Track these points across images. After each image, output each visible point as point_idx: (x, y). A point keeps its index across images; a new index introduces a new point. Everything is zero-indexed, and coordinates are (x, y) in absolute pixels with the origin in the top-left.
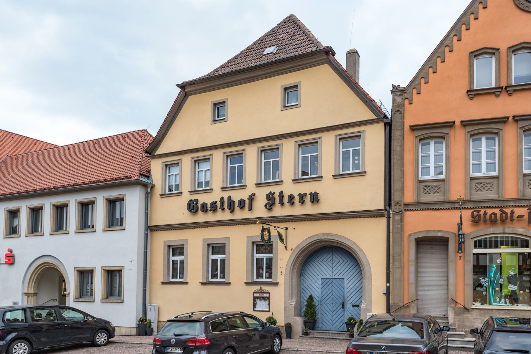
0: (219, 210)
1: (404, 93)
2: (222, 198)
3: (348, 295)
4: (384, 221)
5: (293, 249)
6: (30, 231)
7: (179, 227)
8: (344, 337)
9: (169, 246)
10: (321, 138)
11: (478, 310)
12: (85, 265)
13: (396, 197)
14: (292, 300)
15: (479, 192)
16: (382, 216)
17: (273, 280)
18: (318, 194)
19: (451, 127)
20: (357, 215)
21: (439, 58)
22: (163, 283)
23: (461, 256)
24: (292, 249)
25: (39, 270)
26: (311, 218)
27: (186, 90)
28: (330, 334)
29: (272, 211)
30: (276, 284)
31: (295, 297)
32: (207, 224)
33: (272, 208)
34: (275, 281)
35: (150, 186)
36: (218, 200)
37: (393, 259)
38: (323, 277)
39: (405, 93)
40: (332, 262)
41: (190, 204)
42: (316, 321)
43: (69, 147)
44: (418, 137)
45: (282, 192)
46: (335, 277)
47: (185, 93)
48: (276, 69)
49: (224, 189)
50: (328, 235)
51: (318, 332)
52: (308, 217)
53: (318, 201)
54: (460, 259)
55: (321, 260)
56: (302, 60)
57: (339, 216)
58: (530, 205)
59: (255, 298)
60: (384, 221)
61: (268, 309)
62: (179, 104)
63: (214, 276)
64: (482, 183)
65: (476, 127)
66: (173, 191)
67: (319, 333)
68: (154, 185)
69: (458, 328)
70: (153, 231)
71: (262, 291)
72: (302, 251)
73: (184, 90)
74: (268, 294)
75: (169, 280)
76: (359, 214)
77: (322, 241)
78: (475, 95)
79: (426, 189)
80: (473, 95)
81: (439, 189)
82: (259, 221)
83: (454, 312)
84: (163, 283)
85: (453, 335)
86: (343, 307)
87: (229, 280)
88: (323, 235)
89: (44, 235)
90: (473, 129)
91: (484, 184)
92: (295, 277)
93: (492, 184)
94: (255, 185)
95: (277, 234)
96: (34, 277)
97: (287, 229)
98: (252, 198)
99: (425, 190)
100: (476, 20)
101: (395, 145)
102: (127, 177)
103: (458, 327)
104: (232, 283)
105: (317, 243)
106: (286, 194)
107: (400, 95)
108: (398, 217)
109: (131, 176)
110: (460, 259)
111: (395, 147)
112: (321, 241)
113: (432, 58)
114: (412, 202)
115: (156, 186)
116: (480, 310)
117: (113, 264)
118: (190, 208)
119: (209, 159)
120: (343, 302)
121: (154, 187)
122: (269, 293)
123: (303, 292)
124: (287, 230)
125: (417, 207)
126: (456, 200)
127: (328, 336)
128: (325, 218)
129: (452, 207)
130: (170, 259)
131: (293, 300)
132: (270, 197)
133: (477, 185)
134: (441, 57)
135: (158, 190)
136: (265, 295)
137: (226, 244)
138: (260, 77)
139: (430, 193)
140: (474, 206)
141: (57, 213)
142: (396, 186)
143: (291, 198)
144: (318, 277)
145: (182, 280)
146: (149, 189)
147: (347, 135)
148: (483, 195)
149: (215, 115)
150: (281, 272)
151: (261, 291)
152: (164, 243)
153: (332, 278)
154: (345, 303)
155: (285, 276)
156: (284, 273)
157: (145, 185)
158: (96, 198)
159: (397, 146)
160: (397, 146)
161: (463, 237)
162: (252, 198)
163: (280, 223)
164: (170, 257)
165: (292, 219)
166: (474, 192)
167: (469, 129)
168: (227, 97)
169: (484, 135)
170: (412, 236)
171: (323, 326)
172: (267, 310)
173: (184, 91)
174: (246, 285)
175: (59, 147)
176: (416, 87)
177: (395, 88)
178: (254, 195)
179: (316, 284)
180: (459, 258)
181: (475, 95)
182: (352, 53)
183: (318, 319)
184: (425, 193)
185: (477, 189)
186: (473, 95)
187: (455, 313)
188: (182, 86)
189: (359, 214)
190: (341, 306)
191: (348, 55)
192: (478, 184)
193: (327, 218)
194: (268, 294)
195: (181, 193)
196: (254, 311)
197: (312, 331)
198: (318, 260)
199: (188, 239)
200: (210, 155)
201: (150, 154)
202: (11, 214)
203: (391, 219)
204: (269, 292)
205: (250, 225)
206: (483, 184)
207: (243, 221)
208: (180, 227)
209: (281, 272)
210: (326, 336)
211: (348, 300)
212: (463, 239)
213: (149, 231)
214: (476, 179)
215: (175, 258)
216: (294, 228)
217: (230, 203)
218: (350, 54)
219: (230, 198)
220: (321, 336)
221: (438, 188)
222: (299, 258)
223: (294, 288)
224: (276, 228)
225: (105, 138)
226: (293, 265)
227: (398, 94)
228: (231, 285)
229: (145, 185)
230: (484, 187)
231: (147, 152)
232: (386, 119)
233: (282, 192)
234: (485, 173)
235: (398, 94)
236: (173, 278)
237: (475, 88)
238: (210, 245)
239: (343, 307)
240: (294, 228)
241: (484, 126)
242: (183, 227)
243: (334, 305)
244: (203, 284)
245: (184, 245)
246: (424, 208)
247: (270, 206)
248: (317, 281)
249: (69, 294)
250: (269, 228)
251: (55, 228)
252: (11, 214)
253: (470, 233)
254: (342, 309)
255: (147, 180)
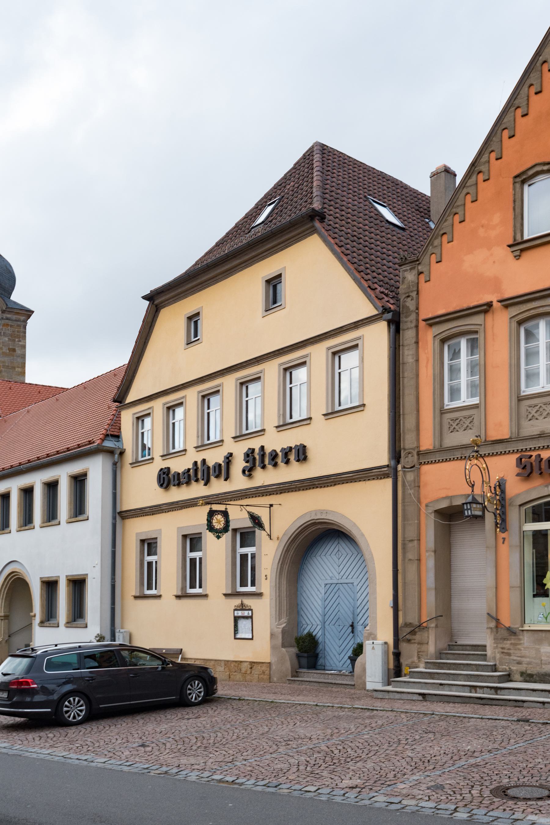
0: (281, 465)
1: (417, 265)
2: (196, 463)
3: (359, 610)
4: (388, 482)
5: (280, 537)
6: (46, 519)
7: (150, 511)
8: (347, 681)
9: (185, 537)
10: (309, 355)
11: (530, 632)
12: (49, 574)
13: (408, 441)
14: (279, 620)
15: (533, 422)
16: (385, 476)
17: (256, 588)
18: (306, 446)
19: (486, 312)
20: (354, 477)
21: (468, 195)
22: (136, 597)
23: (504, 537)
24: (278, 538)
25: (8, 582)
26: (299, 487)
27: (156, 302)
28: (330, 676)
29: (252, 477)
30: (259, 595)
31: (285, 616)
32: (180, 505)
33: (251, 475)
34: (259, 591)
35: (118, 452)
36: (191, 466)
37: (404, 548)
38: (326, 582)
39: (419, 264)
40: (337, 556)
41: (160, 475)
42: (318, 654)
43: (84, 386)
44: (438, 337)
45: (262, 448)
46: (342, 581)
47: (156, 306)
48: (253, 254)
49: (164, 456)
50: (322, 512)
51: (315, 673)
52: (294, 485)
53: (305, 459)
54: (503, 543)
55: (324, 553)
56: (283, 233)
57: (332, 480)
58: (548, 446)
59: (236, 619)
60: (388, 482)
61: (251, 635)
62: (149, 325)
63: (243, 584)
64: (537, 406)
65: (524, 306)
66: (145, 456)
67: (315, 674)
68: (124, 450)
69: (500, 665)
70: (124, 519)
71: (244, 608)
72: (292, 541)
73: (153, 302)
74: (250, 612)
75: (236, 589)
76: (356, 475)
77: (315, 522)
78: (522, 250)
79: (452, 424)
80: (519, 251)
81: (471, 422)
82: (201, 502)
83: (492, 637)
84: (136, 597)
85: (481, 677)
86: (353, 632)
87: (260, 589)
88: (316, 512)
89: (89, 519)
90: (519, 310)
91: (541, 407)
92: (285, 583)
93: (459, 420)
94: (233, 439)
95: (247, 516)
96: (4, 592)
97: (271, 505)
98: (229, 458)
99: (451, 425)
100: (524, 117)
101: (407, 355)
102: (90, 442)
103: (499, 663)
104: (209, 594)
105: (311, 526)
106: (268, 450)
107: (411, 269)
108: (410, 477)
109: (94, 440)
110: (503, 543)
111: (405, 357)
112: (314, 523)
113: (456, 197)
114: (431, 447)
115: (127, 451)
116: (533, 632)
117: (77, 571)
118: (160, 482)
119: (218, 391)
120: (353, 623)
121: (125, 451)
122: (252, 610)
123: (303, 606)
124: (271, 508)
125: (438, 457)
126: (469, 442)
127: (328, 679)
128: (315, 484)
129: (489, 452)
130: (237, 553)
131: (282, 620)
132: (249, 455)
133: (530, 409)
134: (471, 193)
135: (129, 457)
136: (246, 613)
137: (203, 534)
138: (238, 267)
139: (459, 430)
140: (524, 448)
141: (49, 494)
142: (408, 422)
143: (274, 456)
144: (320, 582)
145: (253, 589)
146: (116, 456)
147: (338, 347)
148: (538, 426)
149: (191, 334)
150: (266, 576)
151: (242, 607)
152: (136, 536)
153: (338, 582)
154: (355, 624)
155: (270, 582)
156: (269, 577)
157: (110, 452)
158: (60, 476)
159: (408, 355)
160: (408, 355)
161: (469, 507)
162: (229, 458)
163: (257, 498)
164: (187, 554)
165: (275, 489)
166: (525, 423)
167: (514, 311)
168: (201, 306)
169: (464, 337)
170: (430, 507)
171: (328, 664)
172: (251, 637)
173: (153, 303)
174: (226, 599)
175: (67, 389)
176: (432, 252)
177: (404, 258)
178: (231, 455)
179: (318, 593)
180: (502, 540)
181: (522, 250)
182: (438, 173)
183: (321, 652)
184: (450, 431)
185: (530, 416)
186: (519, 251)
187: (494, 639)
188: (149, 298)
189: (356, 475)
190: (350, 628)
191: (432, 178)
192: (531, 407)
193: (319, 484)
194: (250, 612)
195: (153, 459)
196: (235, 638)
197: (307, 671)
198: (330, 554)
199: (161, 530)
200: (183, 397)
201: (120, 402)
202: (26, 494)
203: (400, 479)
204: (252, 608)
205: (351, 483)
206: (538, 406)
207: (219, 497)
208: (152, 510)
209: (266, 576)
210: (324, 679)
211: (359, 619)
212: (469, 511)
213: (118, 518)
214: (528, 399)
215: (245, 550)
216: (280, 504)
217: (204, 470)
218: (435, 176)
219: (204, 461)
220: (319, 679)
221: (469, 421)
222: (289, 551)
223: (283, 602)
224: (245, 507)
225: (98, 377)
226: (280, 563)
227: (408, 268)
228: (209, 598)
229: (110, 452)
230: (541, 412)
231: (115, 401)
232: (388, 313)
233: (262, 448)
234: (466, 400)
235: (408, 268)
236: (191, 588)
237: (526, 237)
238: (238, 531)
239: (353, 632)
240: (280, 504)
241: (536, 303)
242: (155, 511)
243: (341, 627)
244: (178, 597)
245: (156, 538)
246: (448, 458)
247: (248, 472)
248: (320, 589)
249: (35, 616)
250: (226, 509)
251: (74, 512)
252: (26, 494)
253: (518, 495)
254: (351, 635)
255: (116, 443)
